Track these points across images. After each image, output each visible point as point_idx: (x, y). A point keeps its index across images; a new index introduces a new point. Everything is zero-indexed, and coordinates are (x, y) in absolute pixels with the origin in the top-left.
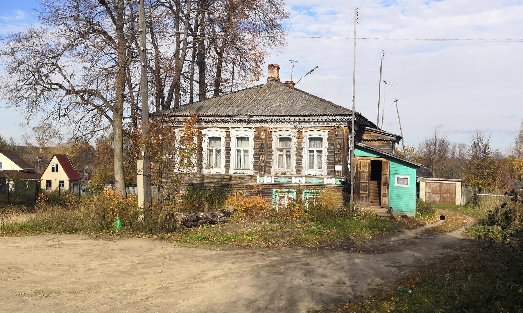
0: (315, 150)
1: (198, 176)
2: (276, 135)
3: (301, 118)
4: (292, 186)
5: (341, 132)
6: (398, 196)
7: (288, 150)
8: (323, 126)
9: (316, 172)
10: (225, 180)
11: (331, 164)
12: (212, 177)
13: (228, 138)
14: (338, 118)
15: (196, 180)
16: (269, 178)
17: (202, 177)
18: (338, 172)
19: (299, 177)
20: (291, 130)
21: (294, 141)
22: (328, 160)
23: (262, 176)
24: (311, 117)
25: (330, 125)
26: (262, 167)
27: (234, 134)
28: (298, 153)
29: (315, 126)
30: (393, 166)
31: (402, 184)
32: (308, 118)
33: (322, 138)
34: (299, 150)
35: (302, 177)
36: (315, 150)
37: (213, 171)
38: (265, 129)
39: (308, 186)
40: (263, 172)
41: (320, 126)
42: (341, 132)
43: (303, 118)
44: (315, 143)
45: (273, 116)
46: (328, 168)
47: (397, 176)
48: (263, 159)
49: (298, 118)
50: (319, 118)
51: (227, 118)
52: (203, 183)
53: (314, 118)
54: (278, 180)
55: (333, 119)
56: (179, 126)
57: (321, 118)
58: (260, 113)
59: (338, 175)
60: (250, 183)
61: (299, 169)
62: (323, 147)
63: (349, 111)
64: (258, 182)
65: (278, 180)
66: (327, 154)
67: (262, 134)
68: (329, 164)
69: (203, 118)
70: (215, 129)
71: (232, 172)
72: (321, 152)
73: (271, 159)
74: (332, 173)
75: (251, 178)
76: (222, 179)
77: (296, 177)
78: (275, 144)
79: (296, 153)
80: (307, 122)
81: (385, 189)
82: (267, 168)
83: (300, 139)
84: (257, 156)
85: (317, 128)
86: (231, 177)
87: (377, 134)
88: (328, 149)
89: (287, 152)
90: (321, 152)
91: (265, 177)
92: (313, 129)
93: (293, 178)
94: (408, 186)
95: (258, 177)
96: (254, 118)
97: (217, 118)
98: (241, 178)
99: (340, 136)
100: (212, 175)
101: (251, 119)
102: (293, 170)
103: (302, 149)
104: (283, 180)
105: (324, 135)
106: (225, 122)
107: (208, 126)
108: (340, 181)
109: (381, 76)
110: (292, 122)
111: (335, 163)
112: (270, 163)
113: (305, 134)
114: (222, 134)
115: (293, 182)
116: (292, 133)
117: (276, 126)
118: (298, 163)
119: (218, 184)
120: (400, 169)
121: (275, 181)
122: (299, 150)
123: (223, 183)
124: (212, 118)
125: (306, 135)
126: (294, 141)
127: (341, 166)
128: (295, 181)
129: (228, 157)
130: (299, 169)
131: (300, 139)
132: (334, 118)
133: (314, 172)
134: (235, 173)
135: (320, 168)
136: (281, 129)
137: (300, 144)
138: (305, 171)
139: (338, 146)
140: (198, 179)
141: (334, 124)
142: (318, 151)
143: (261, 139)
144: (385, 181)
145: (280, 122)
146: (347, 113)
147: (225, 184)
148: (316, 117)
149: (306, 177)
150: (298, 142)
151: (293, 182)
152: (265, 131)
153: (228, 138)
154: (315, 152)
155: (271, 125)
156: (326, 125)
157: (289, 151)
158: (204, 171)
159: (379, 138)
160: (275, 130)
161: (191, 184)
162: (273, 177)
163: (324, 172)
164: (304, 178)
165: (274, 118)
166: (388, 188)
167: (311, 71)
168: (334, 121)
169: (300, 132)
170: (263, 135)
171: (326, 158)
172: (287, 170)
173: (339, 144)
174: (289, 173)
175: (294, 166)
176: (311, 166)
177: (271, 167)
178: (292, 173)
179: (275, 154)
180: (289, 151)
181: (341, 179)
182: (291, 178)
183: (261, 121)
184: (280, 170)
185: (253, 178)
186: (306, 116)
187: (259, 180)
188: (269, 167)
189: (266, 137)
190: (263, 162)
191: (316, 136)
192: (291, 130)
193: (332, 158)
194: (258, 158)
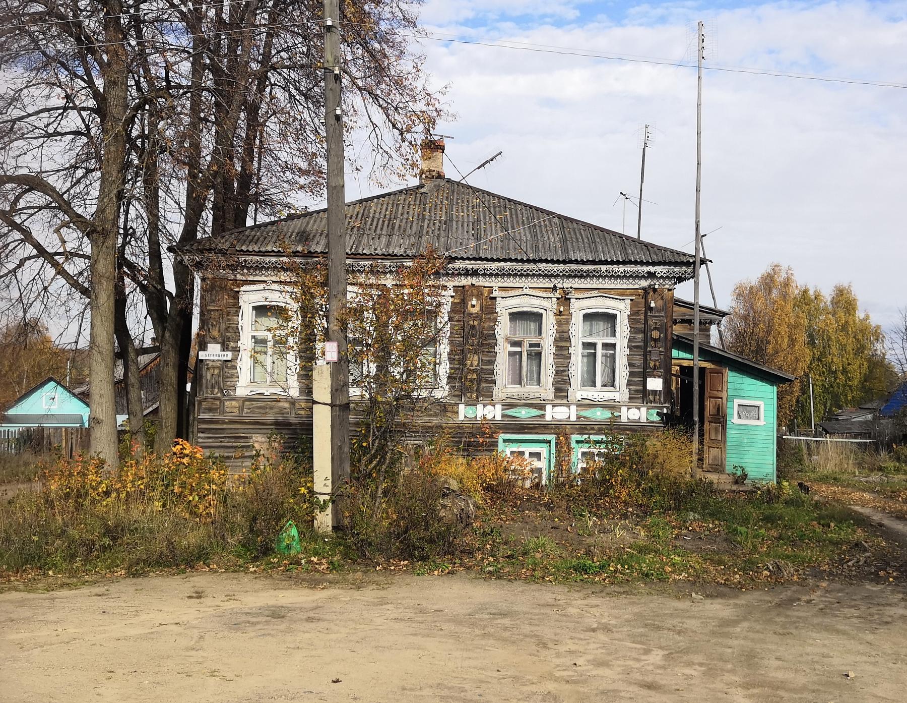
0: (600, 341)
2: (504, 306)
3: (574, 267)
4: (545, 428)
5: (660, 303)
6: (740, 444)
7: (534, 341)
8: (618, 286)
9: (601, 394)
11: (639, 375)
14: (659, 270)
15: (298, 416)
16: (489, 407)
18: (654, 392)
19: (561, 405)
20: (544, 295)
21: (549, 323)
22: (631, 365)
23: (472, 403)
24: (598, 267)
25: (637, 286)
26: (472, 382)
28: (559, 348)
29: (600, 286)
30: (732, 379)
31: (747, 418)
32: (591, 267)
33: (541, 315)
34: (563, 341)
35: (568, 406)
36: (600, 341)
38: (477, 291)
39: (583, 427)
41: (612, 286)
42: (660, 303)
43: (580, 267)
44: (591, 326)
45: (505, 260)
46: (629, 384)
47: (737, 402)
48: (476, 363)
49: (567, 267)
50: (616, 268)
51: (388, 263)
53: (604, 268)
54: (511, 412)
55: (649, 273)
56: (251, 278)
57: (622, 268)
58: (470, 254)
59: (655, 401)
61: (561, 389)
62: (618, 334)
63: (691, 256)
64: (461, 417)
65: (511, 412)
66: (627, 352)
67: (474, 302)
68: (632, 374)
72: (613, 346)
73: (492, 362)
74: (641, 395)
77: (554, 406)
78: (503, 328)
79: (553, 350)
80: (581, 277)
81: (716, 430)
82: (483, 385)
83: (563, 318)
84: (458, 356)
85: (605, 293)
87: (683, 309)
88: (630, 341)
89: (531, 345)
90: (613, 346)
91: (480, 407)
92: (595, 293)
93: (549, 408)
94: (761, 423)
95: (462, 407)
96: (458, 265)
97: (361, 263)
99: (659, 311)
101: (450, 266)
102: (547, 391)
103: (569, 340)
104: (524, 414)
105: (622, 309)
108: (658, 414)
109: (642, 182)
110: (552, 276)
111: (645, 375)
112: (492, 372)
113: (575, 305)
115: (548, 418)
116: (546, 304)
117: (505, 285)
118: (558, 373)
120: (743, 387)
121: (503, 416)
122: (563, 341)
125: (579, 307)
126: (549, 323)
127: (661, 380)
128: (557, 413)
130: (561, 389)
131: (563, 318)
132: (652, 269)
133: (599, 394)
135: (611, 383)
136: (520, 292)
137: (564, 327)
138: (577, 392)
139: (655, 334)
140: (302, 412)
141: (644, 283)
142: (606, 346)
143: (470, 314)
144: (713, 411)
145: (522, 275)
146: (684, 259)
148: (609, 267)
149: (578, 406)
150: (559, 323)
151: (548, 418)
152: (479, 296)
154: (599, 347)
155: (495, 283)
156: (625, 286)
157: (538, 345)
159: (686, 317)
160: (504, 294)
161: (281, 425)
162: (499, 407)
163: (620, 393)
164: (573, 408)
165: (508, 265)
166: (724, 428)
167: (487, 162)
168: (651, 275)
169: (565, 300)
170: (474, 305)
171: (625, 361)
172: (530, 390)
173: (655, 328)
174: (537, 395)
175: (550, 380)
177: (494, 382)
178: (543, 396)
179: (503, 350)
180: (538, 345)
181: (662, 408)
182: (542, 407)
183: (475, 273)
184: (515, 390)
186: (583, 262)
187: (464, 412)
188: (487, 381)
189: (481, 309)
190: (474, 371)
191: (525, 309)
192: (544, 295)
193: (638, 360)
194: (462, 362)
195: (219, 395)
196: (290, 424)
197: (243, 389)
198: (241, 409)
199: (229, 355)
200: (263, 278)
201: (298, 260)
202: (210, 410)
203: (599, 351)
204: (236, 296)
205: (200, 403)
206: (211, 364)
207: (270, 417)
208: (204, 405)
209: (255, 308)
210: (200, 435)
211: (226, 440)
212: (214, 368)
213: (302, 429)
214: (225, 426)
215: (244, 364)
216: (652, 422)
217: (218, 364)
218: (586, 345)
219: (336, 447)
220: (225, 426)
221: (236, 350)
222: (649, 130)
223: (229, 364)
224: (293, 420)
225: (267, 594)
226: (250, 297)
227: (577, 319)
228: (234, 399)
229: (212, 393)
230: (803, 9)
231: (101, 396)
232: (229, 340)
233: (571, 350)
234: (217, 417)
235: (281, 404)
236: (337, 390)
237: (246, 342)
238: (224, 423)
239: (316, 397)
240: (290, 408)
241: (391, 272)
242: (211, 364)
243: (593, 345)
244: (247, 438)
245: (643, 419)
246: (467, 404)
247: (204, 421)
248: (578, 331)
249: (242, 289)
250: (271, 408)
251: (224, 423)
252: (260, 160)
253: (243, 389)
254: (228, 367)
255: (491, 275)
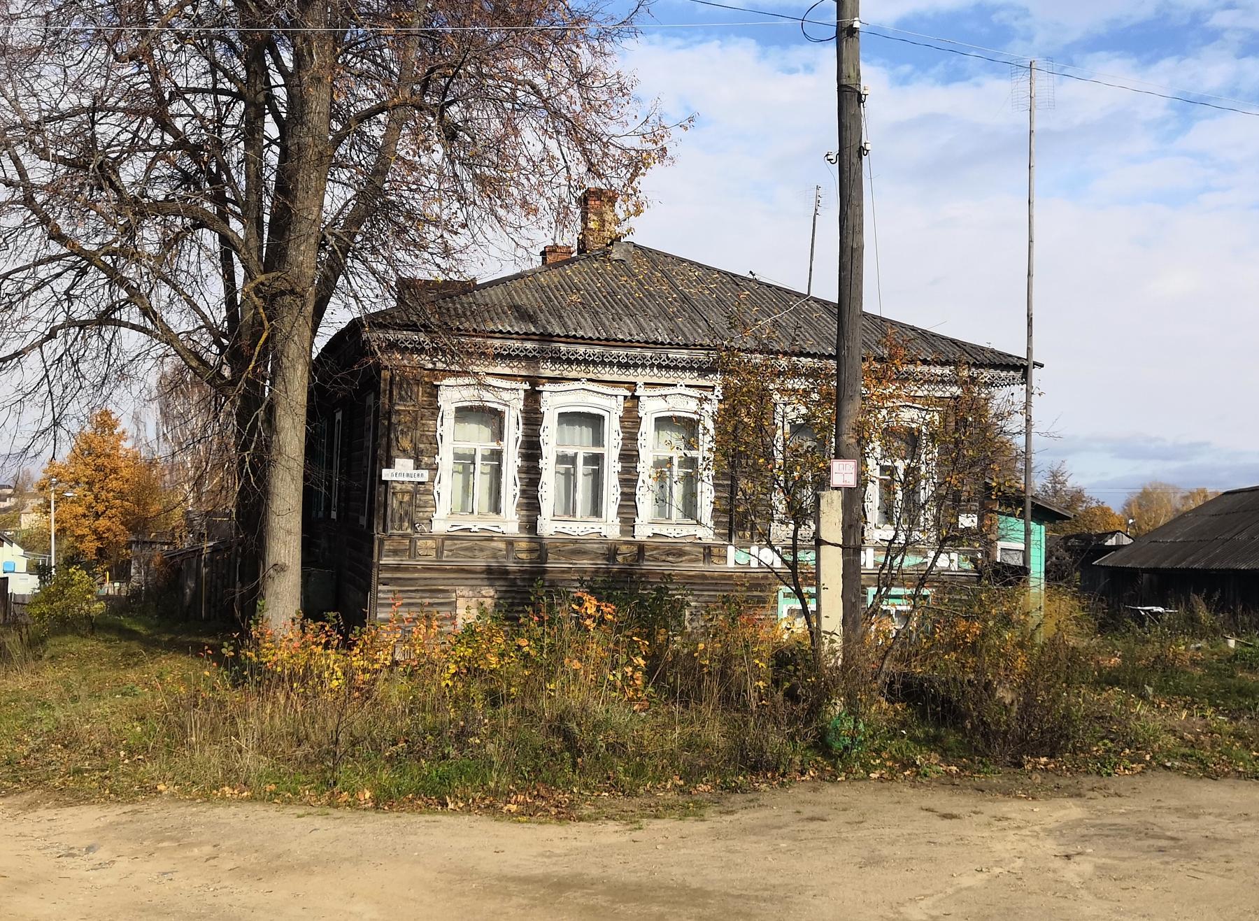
1: (524, 545)
9: (582, 526)
10: (620, 558)
12: (575, 547)
13: (631, 421)
15: (518, 561)
17: (540, 548)
27: (651, 407)
37: (580, 528)
40: (748, 534)
51: (648, 354)
52: (545, 571)
60: (701, 567)
64: (731, 564)
69: (563, 348)
70: (591, 386)
71: (643, 532)
75: (708, 552)
76: (612, 552)
86: (641, 548)
95: (731, 549)
98: (676, 551)
100: (576, 541)
106: (626, 366)
107: (565, 374)
109: (1030, 335)
114: (611, 406)
119: (597, 571)
123: (615, 568)
124: (598, 350)
129: (629, 481)
134: (655, 535)
135: (596, 510)
136: (577, 385)
147: (621, 571)
153: (631, 421)
154: (580, 461)
158: (548, 526)
161: (494, 574)
176: (569, 509)
185: (715, 551)
187: (734, 558)
194: (733, 489)
195: (409, 531)
196: (507, 572)
197: (441, 526)
198: (439, 551)
199: (424, 475)
200: (573, 374)
201: (529, 345)
202: (395, 552)
203: (581, 469)
204: (434, 391)
205: (381, 542)
206: (399, 487)
207: (480, 562)
208: (387, 545)
209: (458, 410)
210: (381, 587)
211: (419, 595)
212: (403, 493)
213: (524, 579)
214: (416, 575)
215: (447, 486)
216: (966, 571)
217: (410, 487)
218: (562, 459)
219: (849, 605)
220: (416, 575)
221: (434, 468)
222: (821, 192)
223: (422, 488)
224: (512, 566)
225: (702, 827)
226: (452, 395)
227: (647, 426)
228: (431, 538)
229: (401, 528)
230: (679, 48)
231: (289, 532)
232: (424, 454)
233: (619, 467)
234: (407, 562)
235: (494, 544)
236: (850, 526)
237: (445, 459)
238: (415, 569)
239: (824, 536)
240: (507, 550)
241: (652, 366)
242: (399, 487)
243: (572, 460)
244: (447, 591)
245: (954, 567)
246: (739, 547)
247: (388, 568)
248: (552, 439)
249: (446, 382)
250: (482, 550)
251: (415, 569)
252: (340, 212)
253: (441, 526)
254: (419, 490)
255: (676, 368)
